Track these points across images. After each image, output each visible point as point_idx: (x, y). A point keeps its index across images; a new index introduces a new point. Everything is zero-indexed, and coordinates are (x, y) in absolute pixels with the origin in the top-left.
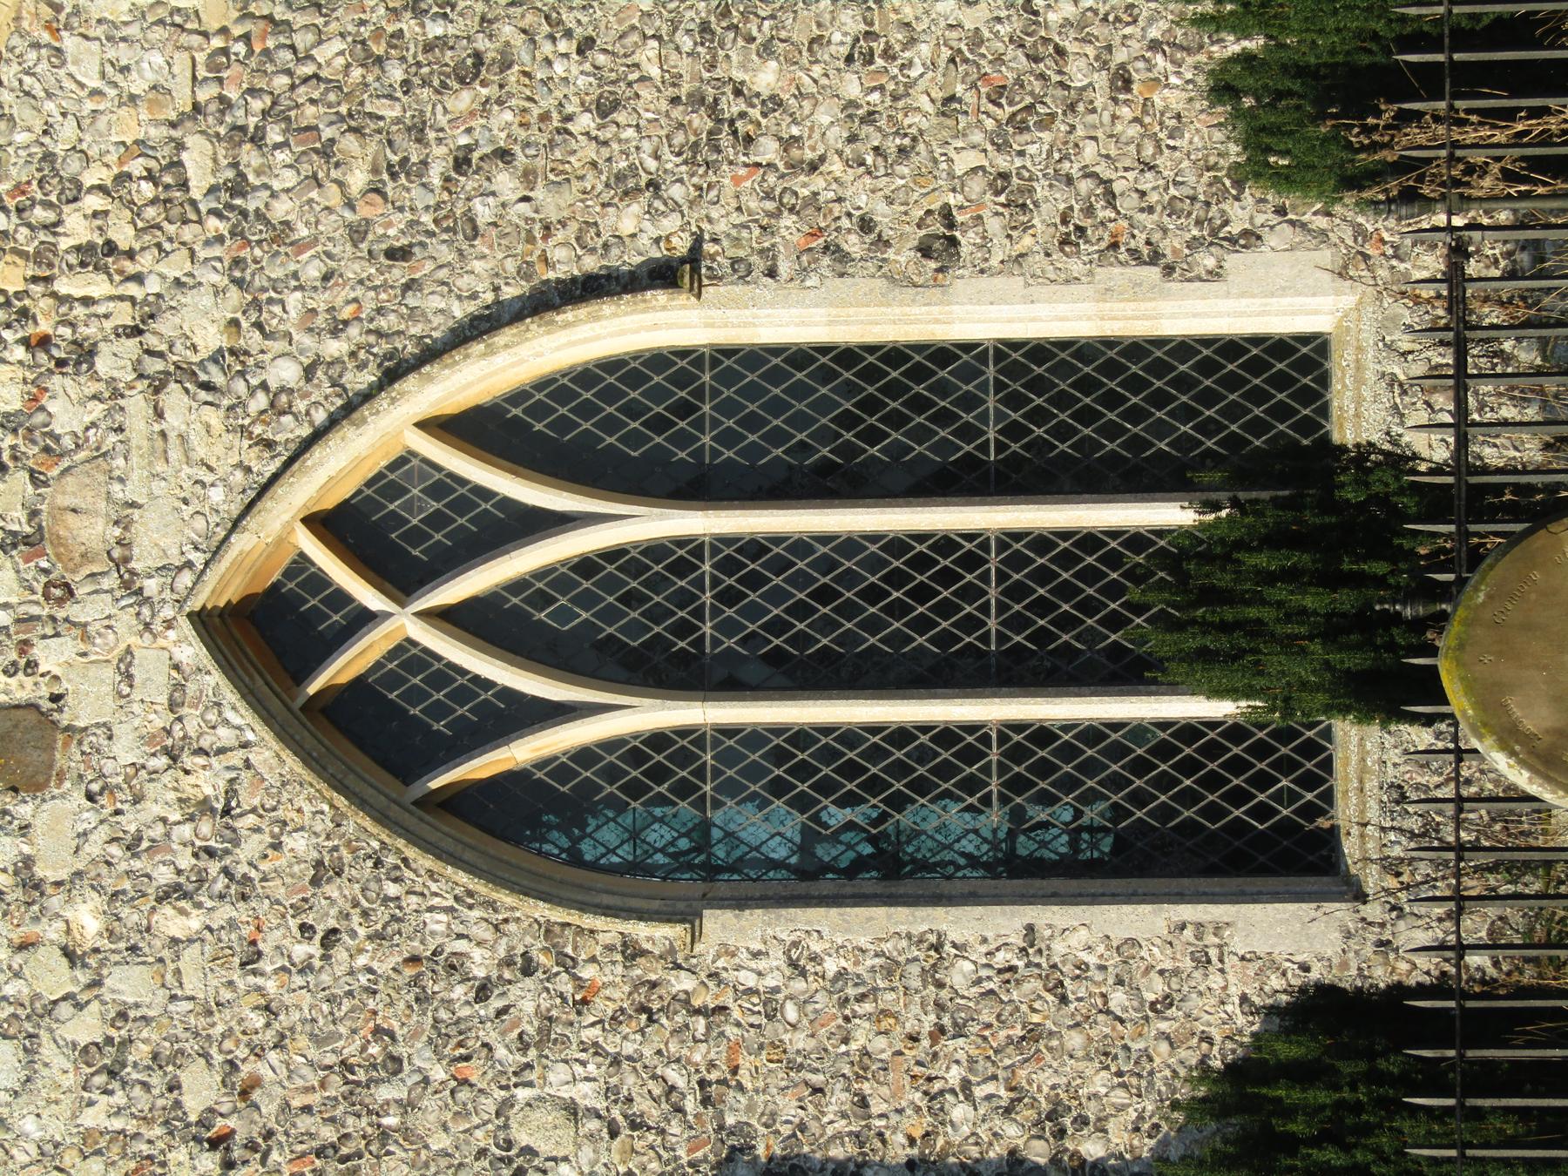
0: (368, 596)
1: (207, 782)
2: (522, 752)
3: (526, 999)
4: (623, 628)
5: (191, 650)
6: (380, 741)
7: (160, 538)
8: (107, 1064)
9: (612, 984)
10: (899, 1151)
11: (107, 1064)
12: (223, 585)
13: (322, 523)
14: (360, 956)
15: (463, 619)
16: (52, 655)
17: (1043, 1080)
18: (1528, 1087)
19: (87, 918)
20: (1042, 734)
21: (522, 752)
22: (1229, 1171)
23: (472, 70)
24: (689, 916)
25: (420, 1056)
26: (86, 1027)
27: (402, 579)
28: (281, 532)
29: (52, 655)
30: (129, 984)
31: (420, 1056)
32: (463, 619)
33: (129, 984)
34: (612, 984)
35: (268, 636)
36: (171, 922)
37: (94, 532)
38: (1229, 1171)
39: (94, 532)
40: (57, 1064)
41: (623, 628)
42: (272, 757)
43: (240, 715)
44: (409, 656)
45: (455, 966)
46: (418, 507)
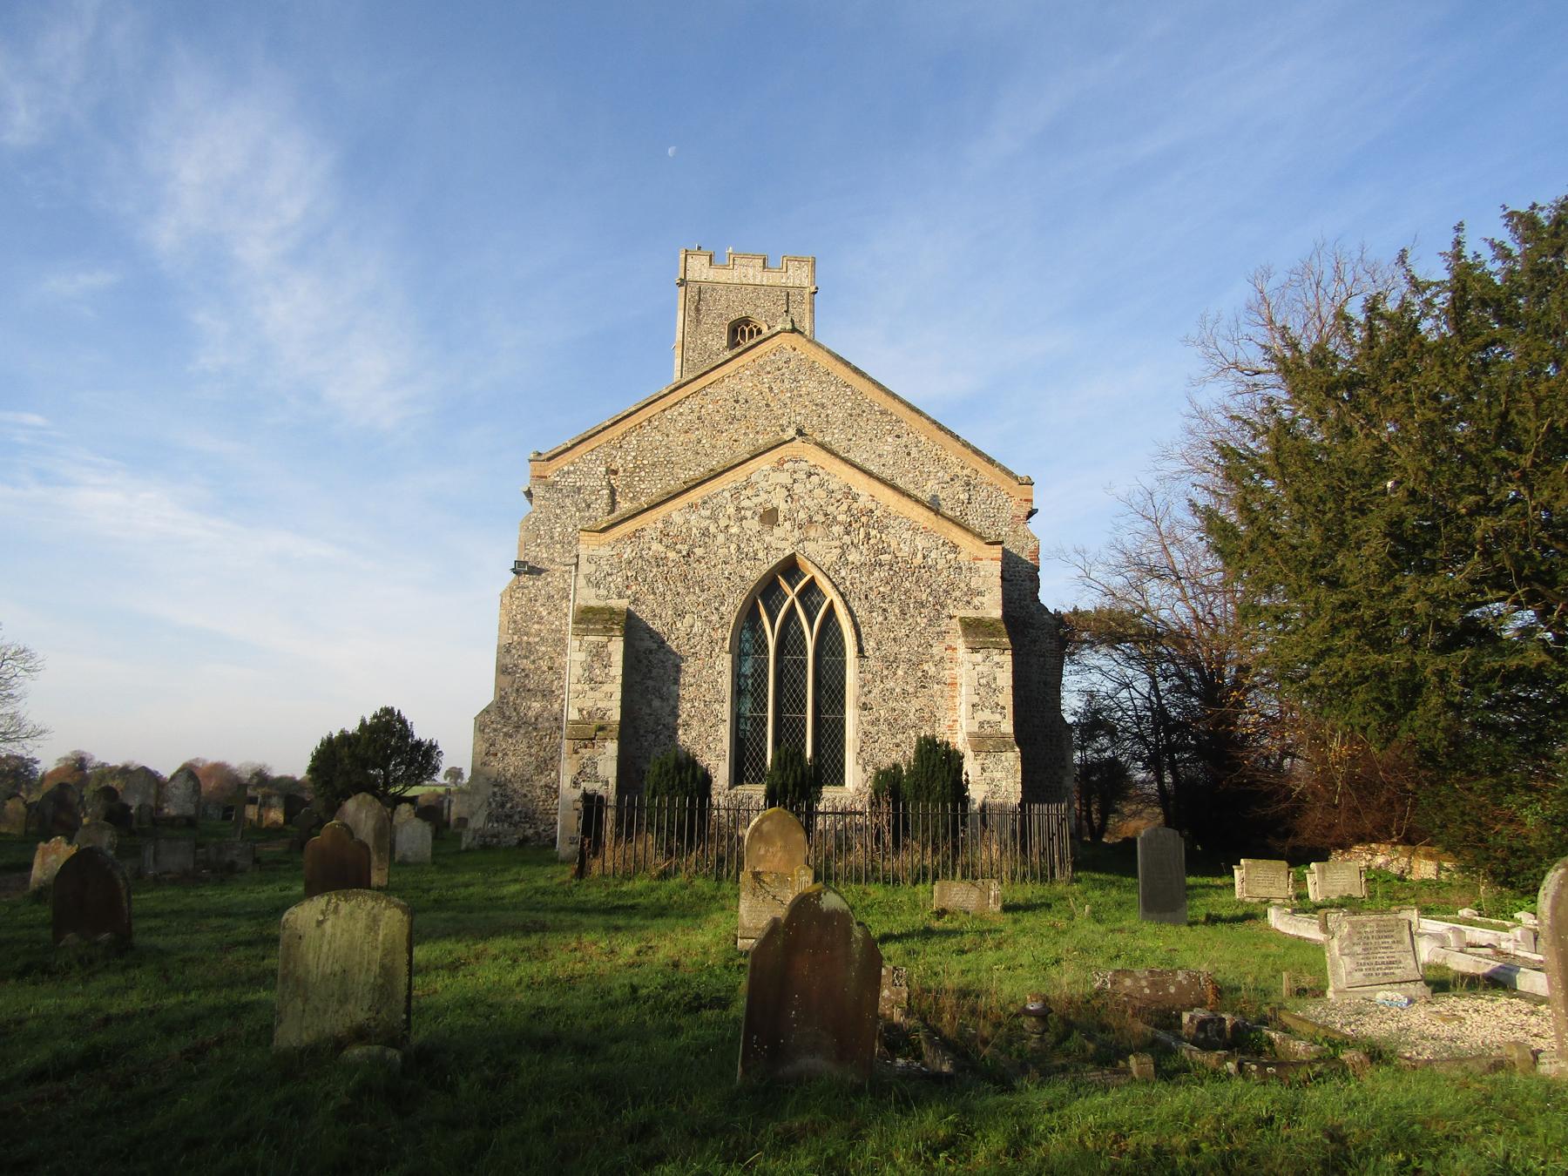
1: (761, 555)
2: (765, 619)
3: (715, 618)
4: (789, 640)
5: (787, 553)
6: (768, 590)
7: (810, 547)
9: (718, 635)
11: (705, 533)
12: (800, 559)
13: (812, 580)
16: (788, 525)
17: (694, 723)
19: (734, 530)
21: (765, 619)
24: (730, 651)
26: (712, 529)
27: (800, 595)
28: (811, 571)
29: (788, 525)
30: (721, 538)
31: (705, 595)
33: (721, 538)
34: (718, 635)
35: (790, 568)
36: (733, 547)
37: (812, 534)
39: (812, 534)
41: (789, 640)
42: (765, 568)
44: (785, 596)
45: (722, 604)
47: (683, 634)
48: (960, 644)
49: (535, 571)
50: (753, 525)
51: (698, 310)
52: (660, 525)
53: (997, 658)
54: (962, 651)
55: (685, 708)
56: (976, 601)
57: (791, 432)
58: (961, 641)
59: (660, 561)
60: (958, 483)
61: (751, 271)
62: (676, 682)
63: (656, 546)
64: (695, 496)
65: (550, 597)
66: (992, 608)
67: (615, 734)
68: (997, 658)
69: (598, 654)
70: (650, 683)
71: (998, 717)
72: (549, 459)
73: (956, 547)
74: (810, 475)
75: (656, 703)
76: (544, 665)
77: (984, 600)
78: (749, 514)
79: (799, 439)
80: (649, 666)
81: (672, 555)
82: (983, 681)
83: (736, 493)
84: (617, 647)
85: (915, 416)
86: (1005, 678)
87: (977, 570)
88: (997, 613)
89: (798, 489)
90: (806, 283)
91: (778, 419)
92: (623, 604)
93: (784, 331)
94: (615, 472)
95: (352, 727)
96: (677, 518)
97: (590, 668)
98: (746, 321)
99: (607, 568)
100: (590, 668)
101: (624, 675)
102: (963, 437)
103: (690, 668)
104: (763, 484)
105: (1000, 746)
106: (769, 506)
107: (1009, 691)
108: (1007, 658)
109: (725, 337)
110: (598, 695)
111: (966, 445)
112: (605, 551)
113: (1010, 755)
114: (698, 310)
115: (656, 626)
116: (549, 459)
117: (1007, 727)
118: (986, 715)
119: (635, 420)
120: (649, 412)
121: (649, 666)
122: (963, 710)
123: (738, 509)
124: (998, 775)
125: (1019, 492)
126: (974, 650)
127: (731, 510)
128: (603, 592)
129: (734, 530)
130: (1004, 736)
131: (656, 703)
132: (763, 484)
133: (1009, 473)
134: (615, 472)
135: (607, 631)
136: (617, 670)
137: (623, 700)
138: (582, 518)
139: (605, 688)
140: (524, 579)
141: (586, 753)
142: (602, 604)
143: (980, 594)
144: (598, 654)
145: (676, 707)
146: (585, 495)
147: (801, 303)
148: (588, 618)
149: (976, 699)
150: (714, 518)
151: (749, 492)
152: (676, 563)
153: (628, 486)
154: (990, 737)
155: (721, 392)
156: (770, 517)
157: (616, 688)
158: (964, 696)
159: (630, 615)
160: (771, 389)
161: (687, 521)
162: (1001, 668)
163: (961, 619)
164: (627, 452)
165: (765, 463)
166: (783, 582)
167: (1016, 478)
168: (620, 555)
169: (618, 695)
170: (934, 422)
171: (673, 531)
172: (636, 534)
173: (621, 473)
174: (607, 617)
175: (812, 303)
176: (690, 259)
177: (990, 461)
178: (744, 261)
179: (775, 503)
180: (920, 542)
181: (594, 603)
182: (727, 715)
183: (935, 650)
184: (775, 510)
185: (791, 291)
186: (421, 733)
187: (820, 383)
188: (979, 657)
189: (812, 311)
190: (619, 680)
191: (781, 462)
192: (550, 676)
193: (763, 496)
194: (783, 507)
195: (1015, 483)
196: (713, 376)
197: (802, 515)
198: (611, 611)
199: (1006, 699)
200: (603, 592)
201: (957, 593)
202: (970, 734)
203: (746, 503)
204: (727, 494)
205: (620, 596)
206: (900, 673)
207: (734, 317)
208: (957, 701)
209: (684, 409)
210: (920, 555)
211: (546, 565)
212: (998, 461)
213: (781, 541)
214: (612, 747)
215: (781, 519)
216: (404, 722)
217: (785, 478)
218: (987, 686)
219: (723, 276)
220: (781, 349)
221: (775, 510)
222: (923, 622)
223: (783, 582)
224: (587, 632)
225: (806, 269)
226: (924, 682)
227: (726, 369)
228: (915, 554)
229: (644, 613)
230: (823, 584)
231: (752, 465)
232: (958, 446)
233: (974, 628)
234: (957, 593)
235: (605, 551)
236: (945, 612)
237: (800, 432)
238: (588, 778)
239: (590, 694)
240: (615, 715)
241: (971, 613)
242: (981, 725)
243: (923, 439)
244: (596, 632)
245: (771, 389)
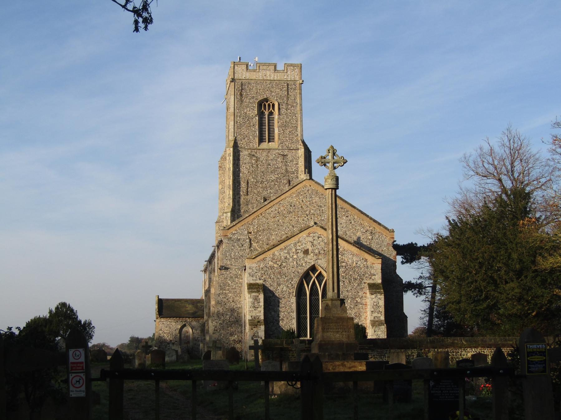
0: (316, 275)
1: (304, 265)
2: (306, 285)
3: (290, 285)
4: (314, 291)
5: (312, 264)
6: (306, 276)
7: (319, 261)
8: (286, 258)
9: (291, 291)
10: (280, 310)
11: (286, 258)
12: (316, 266)
13: (320, 272)
14: (292, 275)
15: (314, 282)
16: (312, 254)
17: (285, 319)
18: (109, 358)
19: (295, 257)
20: (307, 319)
21: (306, 285)
22: (412, 243)
23: (350, 282)
24: (295, 296)
25: (286, 278)
26: (288, 257)
27: (317, 277)
28: (320, 270)
29: (312, 254)
30: (291, 259)
31: (286, 278)
32: (314, 282)
33: (291, 259)
34: (291, 291)
35: (313, 269)
36: (295, 263)
37: (320, 257)
38: (412, 243)
39: (320, 257)
40: (286, 255)
41: (314, 291)
42: (306, 269)
43: (308, 267)
44: (312, 278)
45: (292, 281)
46: (321, 278)
47: (280, 291)
48: (368, 291)
49: (227, 269)
50: (301, 255)
51: (241, 95)
52: (271, 256)
53: (379, 297)
54: (368, 294)
55: (282, 315)
56: (373, 277)
57: (313, 223)
58: (368, 291)
59: (272, 268)
60: (368, 233)
61: (268, 73)
62: (279, 306)
63: (270, 263)
64: (282, 246)
65: (231, 277)
66: (378, 280)
67: (263, 323)
68: (379, 297)
69: (256, 299)
70: (271, 307)
71: (379, 315)
72: (228, 229)
73: (366, 260)
74: (319, 238)
75: (273, 313)
76: (231, 300)
77: (376, 277)
78: (300, 251)
79: (315, 226)
80: (271, 303)
81: (275, 266)
82: (375, 304)
83: (295, 245)
84: (261, 297)
85: (353, 209)
86: (382, 303)
87: (373, 267)
88: (380, 281)
89: (315, 242)
90: (297, 78)
91: (305, 212)
92: (261, 282)
93: (307, 179)
94: (251, 233)
95: (45, 314)
96: (277, 253)
97: (254, 303)
98: (266, 100)
99: (255, 271)
100: (254, 303)
101: (264, 305)
102: (370, 215)
103: (283, 302)
104: (304, 241)
105: (380, 324)
106: (306, 248)
107: (383, 307)
108: (382, 297)
109: (256, 109)
110: (257, 311)
111: (371, 219)
112: (255, 265)
113: (383, 327)
114: (241, 95)
115: (271, 288)
116: (228, 229)
117: (383, 318)
118: (376, 314)
119: (256, 214)
120: (261, 211)
121: (271, 303)
122: (369, 313)
123: (296, 250)
124: (379, 333)
125: (389, 235)
126: (372, 294)
127: (294, 250)
128: (254, 278)
129: (295, 257)
130: (381, 321)
131: (273, 313)
132: (304, 241)
133: (386, 228)
134: (251, 233)
135: (258, 292)
136: (262, 304)
137: (264, 313)
138: (241, 250)
139: (259, 309)
140: (223, 271)
141: (255, 329)
142: (254, 282)
143: (374, 275)
144: (256, 299)
145: (279, 314)
146: (241, 241)
147: (295, 89)
148: (252, 287)
149: (373, 309)
150: (288, 253)
151: (299, 244)
152: (277, 268)
153: (255, 238)
154: (377, 321)
155: (285, 203)
156: (306, 252)
157: (262, 309)
158: (369, 309)
159: (264, 285)
160: (303, 201)
161: (280, 254)
162: (380, 300)
163: (368, 284)
164: (254, 226)
165: (304, 234)
166: (311, 273)
167: (388, 230)
168: (259, 266)
169: (262, 311)
170: (360, 211)
171: (276, 258)
172: (264, 259)
173: (252, 233)
174: (257, 287)
175: (301, 89)
176: (236, 68)
177: (380, 224)
178: (265, 67)
179: (308, 247)
180: (355, 259)
181: (252, 282)
182: (295, 316)
183: (360, 294)
184: (308, 250)
185: (290, 83)
186: (82, 317)
187: (320, 198)
188: (373, 296)
189: (301, 94)
190: (263, 307)
191: (309, 234)
192: (233, 304)
193: (304, 245)
194: (310, 249)
195: (388, 232)
196: (282, 197)
197: (317, 251)
198: (257, 284)
199: (382, 309)
200: (254, 278)
201: (367, 275)
202: (371, 321)
203: (298, 248)
204: (292, 245)
205: (260, 280)
206: (349, 301)
207: (260, 98)
208: (367, 310)
209: (273, 209)
210: (355, 263)
211: (230, 266)
212: (382, 223)
213: (310, 260)
214: (263, 327)
215: (310, 252)
216: (72, 310)
217: (311, 239)
218: (376, 306)
219: (254, 76)
220: (306, 186)
221: (308, 250)
222: (356, 285)
223: (311, 273)
224: (252, 292)
225: (297, 70)
226: (357, 304)
227: (287, 194)
228: (353, 263)
229: (268, 285)
230: (324, 273)
231: (300, 235)
232: (368, 219)
233: (373, 287)
234: (367, 275)
235: (255, 265)
236: (363, 282)
237: (315, 223)
238: (256, 337)
239: (254, 311)
240: (262, 318)
241: (371, 282)
242: (374, 317)
243: (356, 217)
244: (254, 292)
245: (303, 201)
